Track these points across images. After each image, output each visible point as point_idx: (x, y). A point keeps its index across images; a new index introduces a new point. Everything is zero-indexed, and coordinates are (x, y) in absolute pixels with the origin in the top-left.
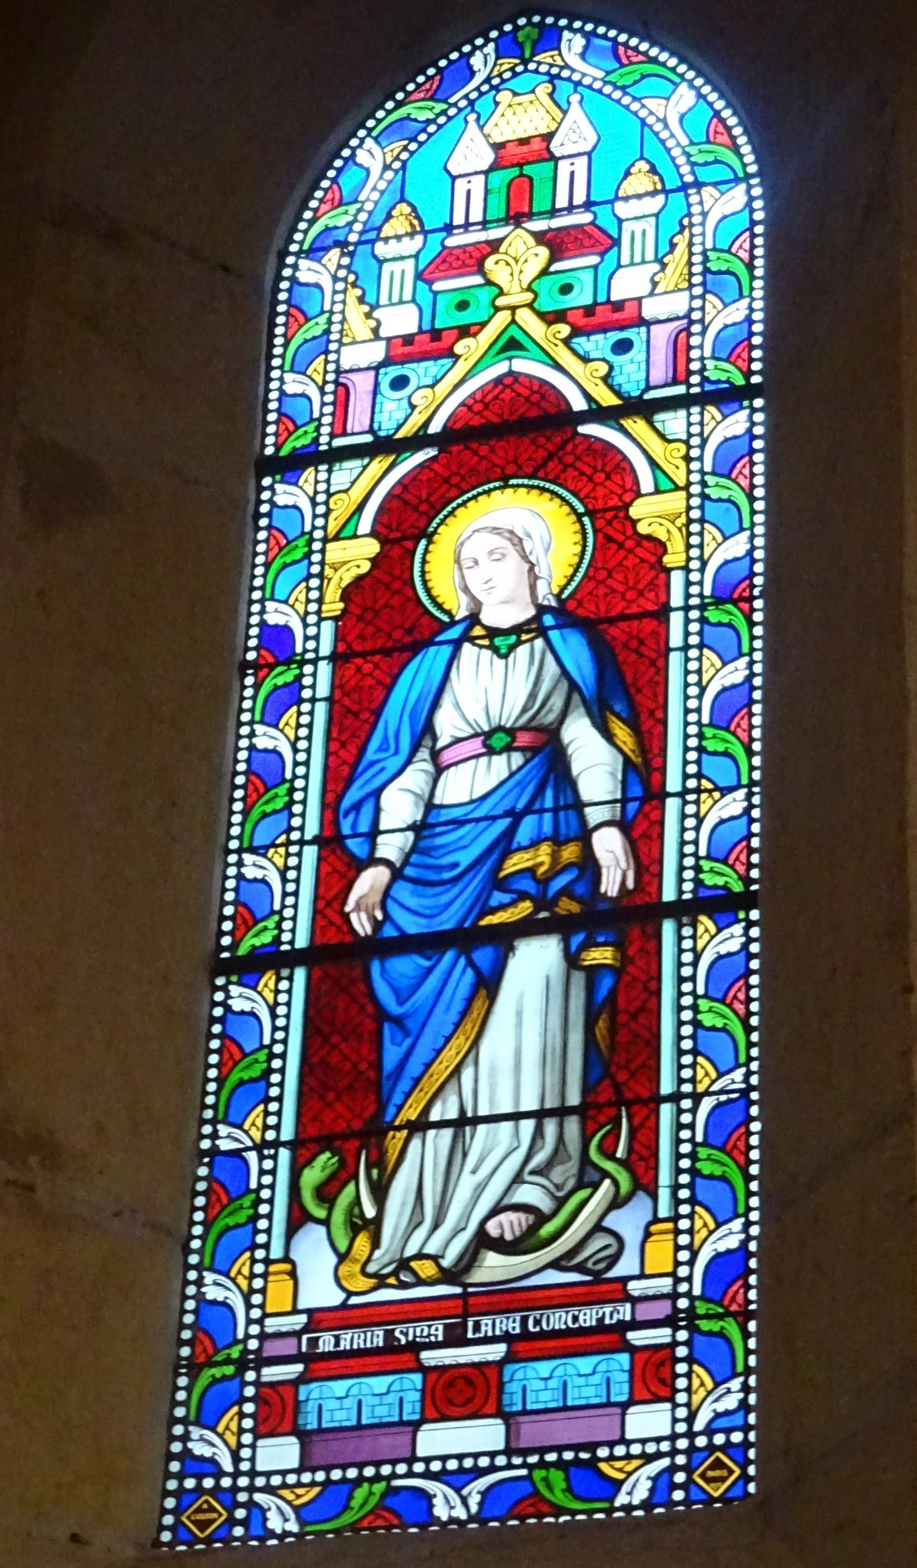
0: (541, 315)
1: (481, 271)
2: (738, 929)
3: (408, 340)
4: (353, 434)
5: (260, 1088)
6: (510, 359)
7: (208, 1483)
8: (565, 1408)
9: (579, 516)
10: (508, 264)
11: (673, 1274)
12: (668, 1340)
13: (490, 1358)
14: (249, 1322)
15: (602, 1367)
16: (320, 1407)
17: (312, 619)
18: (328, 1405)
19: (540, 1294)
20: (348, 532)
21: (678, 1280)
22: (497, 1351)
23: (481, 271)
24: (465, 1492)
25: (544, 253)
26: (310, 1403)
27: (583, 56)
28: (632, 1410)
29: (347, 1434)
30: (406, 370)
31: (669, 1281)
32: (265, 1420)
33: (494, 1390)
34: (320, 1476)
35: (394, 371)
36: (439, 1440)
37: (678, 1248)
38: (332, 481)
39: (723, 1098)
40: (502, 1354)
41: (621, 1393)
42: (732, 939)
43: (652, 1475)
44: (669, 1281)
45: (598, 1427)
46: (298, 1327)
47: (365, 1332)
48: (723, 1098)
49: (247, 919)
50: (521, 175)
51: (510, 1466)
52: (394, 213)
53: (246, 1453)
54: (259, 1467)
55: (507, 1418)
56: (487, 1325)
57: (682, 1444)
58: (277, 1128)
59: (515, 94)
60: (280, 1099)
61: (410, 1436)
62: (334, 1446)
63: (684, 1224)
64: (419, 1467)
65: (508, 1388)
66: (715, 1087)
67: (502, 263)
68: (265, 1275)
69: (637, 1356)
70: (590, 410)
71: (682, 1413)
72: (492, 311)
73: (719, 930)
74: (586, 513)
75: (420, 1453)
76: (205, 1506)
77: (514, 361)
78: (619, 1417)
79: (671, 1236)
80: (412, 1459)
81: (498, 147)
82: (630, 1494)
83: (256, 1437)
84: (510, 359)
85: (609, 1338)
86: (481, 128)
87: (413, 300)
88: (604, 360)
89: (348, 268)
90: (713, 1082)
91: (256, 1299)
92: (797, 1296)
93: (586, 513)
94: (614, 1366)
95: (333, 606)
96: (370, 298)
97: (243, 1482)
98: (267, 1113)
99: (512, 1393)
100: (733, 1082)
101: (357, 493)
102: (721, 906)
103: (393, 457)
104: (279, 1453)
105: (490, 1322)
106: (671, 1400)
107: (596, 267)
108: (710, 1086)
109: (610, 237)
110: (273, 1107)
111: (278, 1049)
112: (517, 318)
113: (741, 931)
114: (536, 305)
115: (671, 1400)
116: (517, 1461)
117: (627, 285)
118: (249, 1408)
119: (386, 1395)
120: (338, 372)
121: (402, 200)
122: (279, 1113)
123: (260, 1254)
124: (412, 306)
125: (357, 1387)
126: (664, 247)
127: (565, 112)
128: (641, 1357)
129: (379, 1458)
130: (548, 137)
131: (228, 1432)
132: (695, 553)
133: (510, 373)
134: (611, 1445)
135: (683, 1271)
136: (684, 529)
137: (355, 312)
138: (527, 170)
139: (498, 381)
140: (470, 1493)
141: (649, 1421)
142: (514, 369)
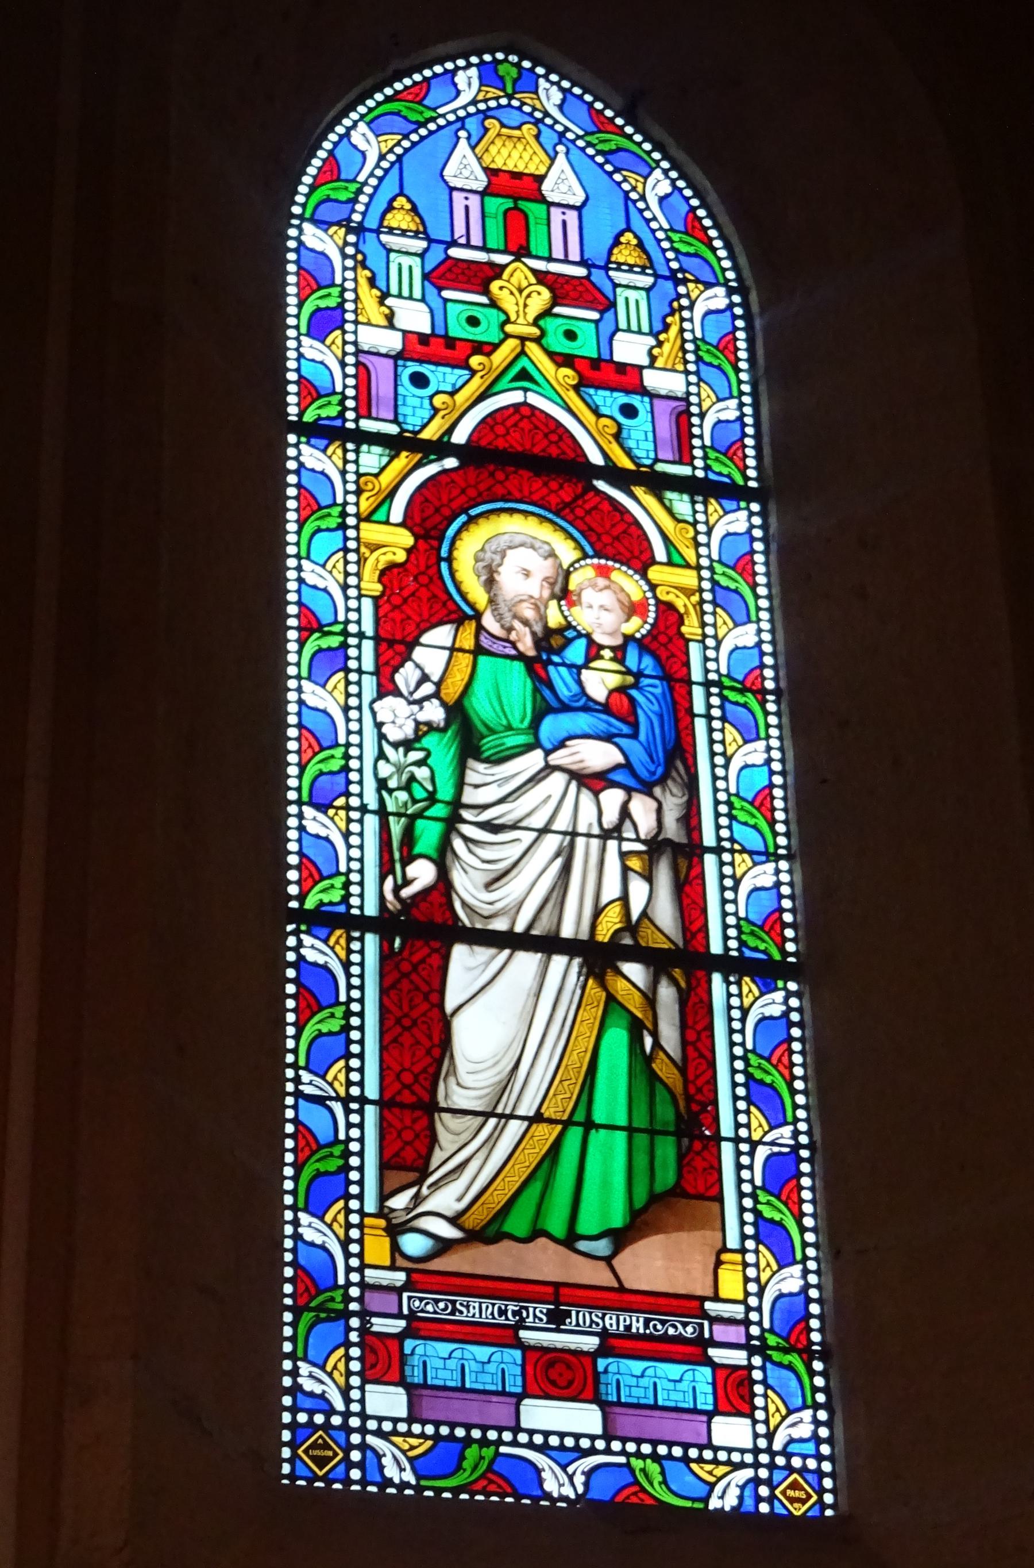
0: (552, 355)
1: (486, 291)
2: (779, 996)
3: (423, 339)
4: (377, 419)
5: (342, 1045)
6: (526, 390)
7: (319, 1419)
8: (655, 1407)
9: (450, 560)
10: (512, 293)
11: (744, 1302)
12: (745, 1363)
13: (585, 1348)
14: (349, 1269)
15: (457, 1354)
16: (618, 1382)
17: (352, 592)
18: (433, 1363)
19: (580, 1293)
20: (380, 515)
21: (749, 1309)
22: (590, 1343)
23: (486, 291)
24: (570, 1469)
25: (546, 294)
26: (416, 1357)
27: (561, 107)
28: (526, 1401)
29: (451, 1394)
30: (426, 369)
31: (741, 1308)
32: (373, 1366)
33: (590, 1380)
34: (430, 1430)
35: (413, 367)
36: (542, 1414)
37: (747, 1280)
38: (361, 462)
39: (776, 1149)
40: (596, 1347)
41: (515, 1385)
42: (773, 1004)
43: (740, 1484)
44: (741, 1308)
45: (691, 1429)
46: (399, 1284)
47: (494, 1305)
48: (776, 1149)
49: (313, 874)
50: (516, 208)
51: (608, 1451)
52: (396, 204)
53: (355, 1394)
54: (750, 1446)
55: (604, 1406)
56: (474, 1308)
57: (355, 1422)
58: (361, 1084)
59: (503, 125)
60: (361, 1056)
61: (513, 1409)
62: (456, 1404)
63: (750, 1258)
64: (523, 1438)
65: (603, 1378)
66: (768, 1138)
67: (534, 295)
68: (361, 1226)
69: (528, 1354)
70: (606, 466)
71: (761, 1429)
72: (502, 336)
73: (762, 994)
74: (440, 559)
75: (524, 1424)
76: (320, 1441)
77: (529, 394)
78: (705, 1425)
79: (740, 1268)
80: (517, 1429)
81: (491, 173)
82: (722, 1497)
83: (365, 1381)
84: (526, 390)
85: (694, 1351)
86: (473, 148)
87: (423, 300)
88: (611, 418)
89: (355, 245)
90: (766, 1133)
91: (354, 1248)
92: (865, 1346)
93: (440, 559)
94: (507, 1358)
95: (373, 586)
96: (381, 283)
97: (764, 1458)
98: (349, 1069)
99: (607, 1384)
100: (782, 1137)
101: (387, 479)
102: (766, 973)
103: (420, 456)
104: (387, 1401)
105: (477, 1305)
106: (751, 1416)
107: (597, 322)
108: (763, 1136)
109: (607, 298)
110: (355, 1063)
111: (355, 1007)
112: (526, 349)
113: (781, 1000)
114: (544, 342)
115: (751, 1416)
116: (616, 1446)
117: (629, 349)
118: (355, 1352)
119: (492, 1366)
120: (358, 352)
121: (401, 193)
122: (361, 1070)
123: (354, 1204)
124: (422, 306)
125: (652, 1369)
126: (658, 326)
127: (553, 160)
128: (533, 1356)
129: (673, 1439)
130: (540, 179)
131: (335, 1372)
132: (710, 631)
133: (525, 404)
134: (701, 1448)
135: (753, 1301)
136: (698, 607)
137: (368, 297)
138: (523, 205)
139: (516, 407)
140: (574, 1473)
141: (731, 1432)
142: (529, 401)
